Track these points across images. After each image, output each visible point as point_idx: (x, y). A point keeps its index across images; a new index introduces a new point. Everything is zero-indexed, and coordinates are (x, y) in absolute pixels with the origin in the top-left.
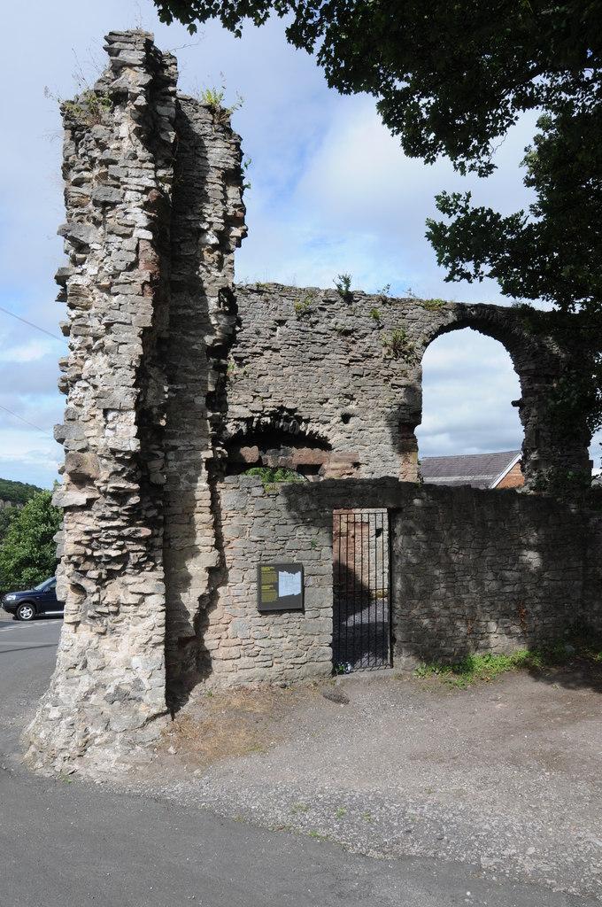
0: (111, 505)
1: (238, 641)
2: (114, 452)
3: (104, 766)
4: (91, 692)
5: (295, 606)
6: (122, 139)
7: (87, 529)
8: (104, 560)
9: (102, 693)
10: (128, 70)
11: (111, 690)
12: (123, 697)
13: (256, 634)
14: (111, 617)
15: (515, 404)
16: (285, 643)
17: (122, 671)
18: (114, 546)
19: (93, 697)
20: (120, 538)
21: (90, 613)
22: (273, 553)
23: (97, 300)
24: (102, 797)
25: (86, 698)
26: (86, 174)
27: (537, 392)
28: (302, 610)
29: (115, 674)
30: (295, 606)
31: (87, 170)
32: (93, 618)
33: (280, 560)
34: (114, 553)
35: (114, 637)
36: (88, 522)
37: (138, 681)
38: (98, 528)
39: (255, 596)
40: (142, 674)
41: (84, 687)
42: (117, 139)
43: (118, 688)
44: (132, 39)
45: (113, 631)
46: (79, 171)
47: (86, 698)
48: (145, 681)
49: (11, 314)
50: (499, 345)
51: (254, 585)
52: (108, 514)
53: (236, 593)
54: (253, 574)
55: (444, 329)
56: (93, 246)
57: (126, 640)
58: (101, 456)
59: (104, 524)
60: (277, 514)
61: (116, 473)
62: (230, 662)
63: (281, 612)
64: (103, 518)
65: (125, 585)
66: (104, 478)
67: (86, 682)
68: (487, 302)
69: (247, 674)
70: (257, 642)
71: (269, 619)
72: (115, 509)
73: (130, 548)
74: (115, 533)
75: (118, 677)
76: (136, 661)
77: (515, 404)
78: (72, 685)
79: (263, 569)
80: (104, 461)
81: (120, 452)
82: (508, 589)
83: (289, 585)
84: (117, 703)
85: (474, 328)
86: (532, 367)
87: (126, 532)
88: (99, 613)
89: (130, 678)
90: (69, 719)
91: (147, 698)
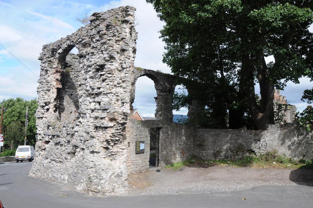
0: (120, 126)
1: (131, 161)
2: (124, 113)
3: (121, 193)
4: (112, 175)
5: (142, 152)
6: (126, 33)
7: (113, 132)
8: (115, 140)
9: (114, 175)
10: (130, 16)
11: (116, 174)
12: (119, 176)
13: (135, 159)
14: (115, 155)
15: (155, 98)
16: (140, 161)
17: (118, 169)
18: (118, 137)
19: (112, 176)
20: (119, 135)
21: (109, 155)
22: (139, 138)
23: (116, 73)
24: (121, 199)
25: (111, 177)
26: (112, 38)
27: (162, 95)
28: (144, 153)
29: (117, 170)
30: (142, 152)
31: (112, 37)
32: (109, 156)
33: (140, 140)
34: (117, 139)
35: (114, 161)
36: (113, 131)
37: (122, 171)
38: (115, 132)
39: (135, 150)
40: (122, 170)
41: (110, 174)
42: (125, 32)
43: (117, 173)
44: (132, 9)
45: (114, 159)
46: (109, 37)
47: (111, 177)
48: (123, 171)
49: (13, 55)
50: (153, 81)
51: (135, 147)
52: (119, 129)
53: (131, 149)
54: (135, 143)
55: (141, 76)
56: (116, 59)
57: (118, 161)
58: (120, 114)
59: (117, 131)
60: (140, 129)
61: (123, 118)
62: (130, 167)
63: (140, 153)
64: (117, 130)
65: (118, 147)
66: (120, 120)
67: (110, 173)
68: (151, 69)
69: (132, 170)
70: (135, 161)
71: (138, 155)
72: (120, 127)
73: (121, 137)
74: (119, 133)
75: (118, 171)
76: (121, 166)
77: (155, 98)
78: (107, 174)
79: (137, 142)
80: (120, 115)
81: (126, 113)
82: (181, 147)
83: (142, 146)
84: (117, 178)
85: (147, 76)
86: (161, 88)
87: (121, 133)
88: (111, 154)
89: (120, 171)
90: (108, 182)
91: (123, 175)
